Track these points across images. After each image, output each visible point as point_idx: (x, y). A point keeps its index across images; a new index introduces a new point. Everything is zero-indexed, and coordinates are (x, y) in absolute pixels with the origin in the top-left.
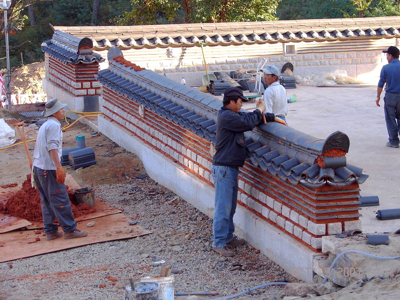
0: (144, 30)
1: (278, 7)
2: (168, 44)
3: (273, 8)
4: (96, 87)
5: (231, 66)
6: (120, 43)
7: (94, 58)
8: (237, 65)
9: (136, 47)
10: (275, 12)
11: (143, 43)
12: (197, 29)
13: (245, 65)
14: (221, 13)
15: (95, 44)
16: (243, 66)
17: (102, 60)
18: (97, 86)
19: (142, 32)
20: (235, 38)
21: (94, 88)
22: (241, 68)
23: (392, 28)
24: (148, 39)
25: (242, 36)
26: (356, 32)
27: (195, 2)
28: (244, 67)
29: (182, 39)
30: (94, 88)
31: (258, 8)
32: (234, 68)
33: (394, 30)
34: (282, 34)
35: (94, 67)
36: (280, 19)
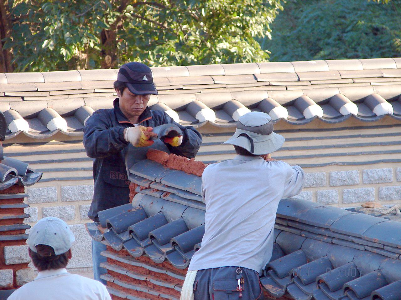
0: (86, 86)
1: (278, 18)
2: (49, 135)
3: (260, 24)
4: (17, 262)
5: (343, 193)
6: (208, 115)
7: (13, 173)
8: (360, 189)
9: (69, 136)
10: (268, 33)
11: (49, 126)
12: (241, 80)
13: (385, 190)
14: (105, 38)
15: (21, 125)
16: (379, 191)
17: (33, 176)
18: (20, 258)
19: (80, 91)
20: (213, 112)
21: (10, 266)
22: (372, 199)
23: (335, 96)
24: (25, 116)
25: (236, 108)
26: (365, 103)
27: (11, 3)
28: (380, 197)
29: (310, 108)
30: (10, 266)
31: (216, 22)
32: (353, 199)
33: (344, 103)
34: (174, 110)
35: (9, 201)
36: (273, 58)
